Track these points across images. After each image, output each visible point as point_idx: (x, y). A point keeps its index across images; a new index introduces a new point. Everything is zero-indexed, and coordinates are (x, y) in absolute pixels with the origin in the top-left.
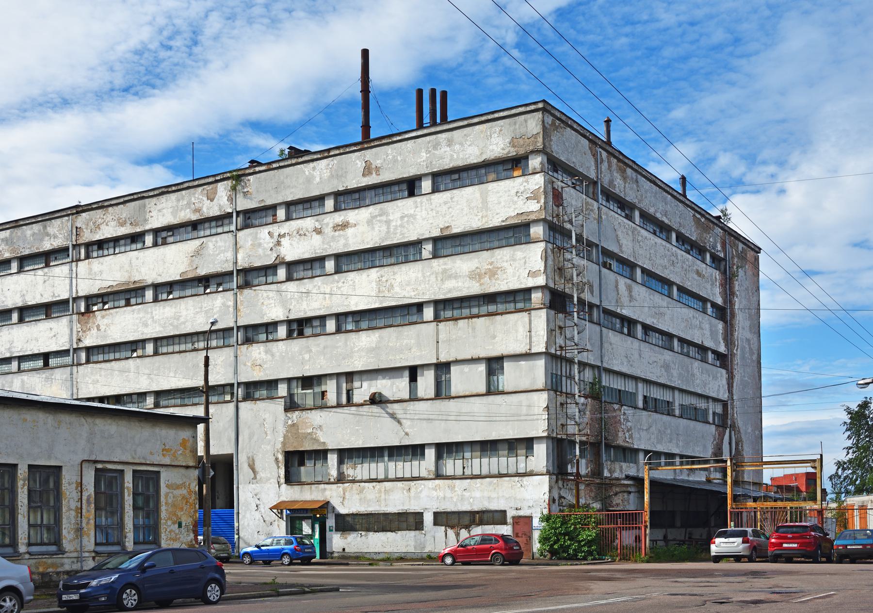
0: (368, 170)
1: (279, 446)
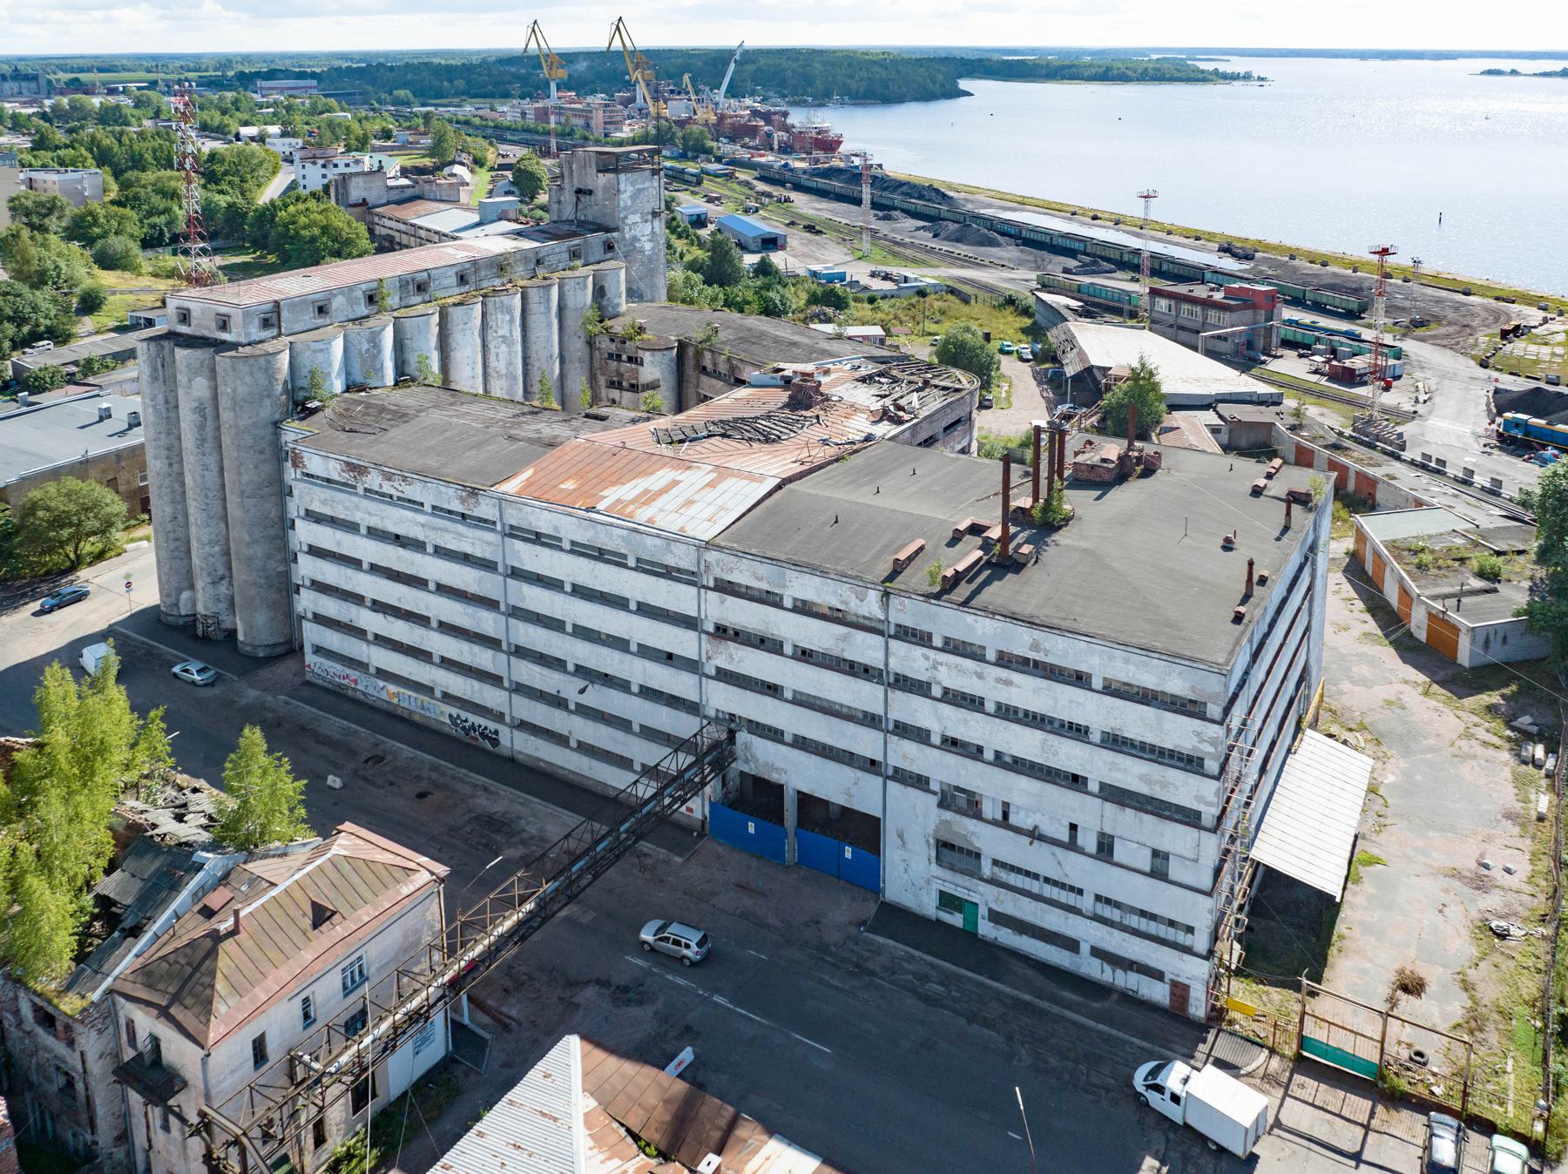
0: (1035, 646)
1: (931, 829)
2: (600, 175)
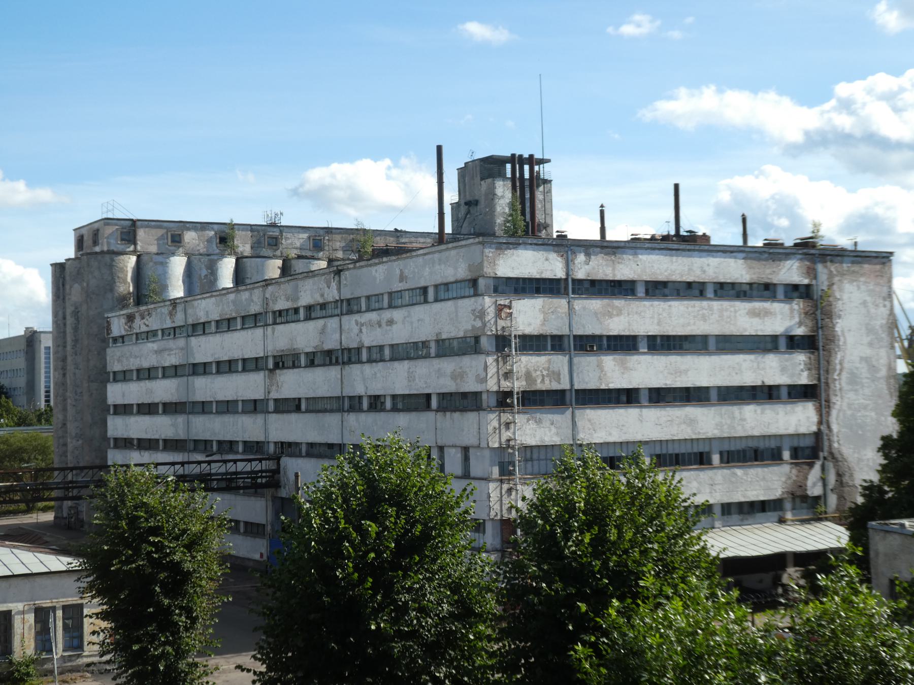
2: (483, 182)
